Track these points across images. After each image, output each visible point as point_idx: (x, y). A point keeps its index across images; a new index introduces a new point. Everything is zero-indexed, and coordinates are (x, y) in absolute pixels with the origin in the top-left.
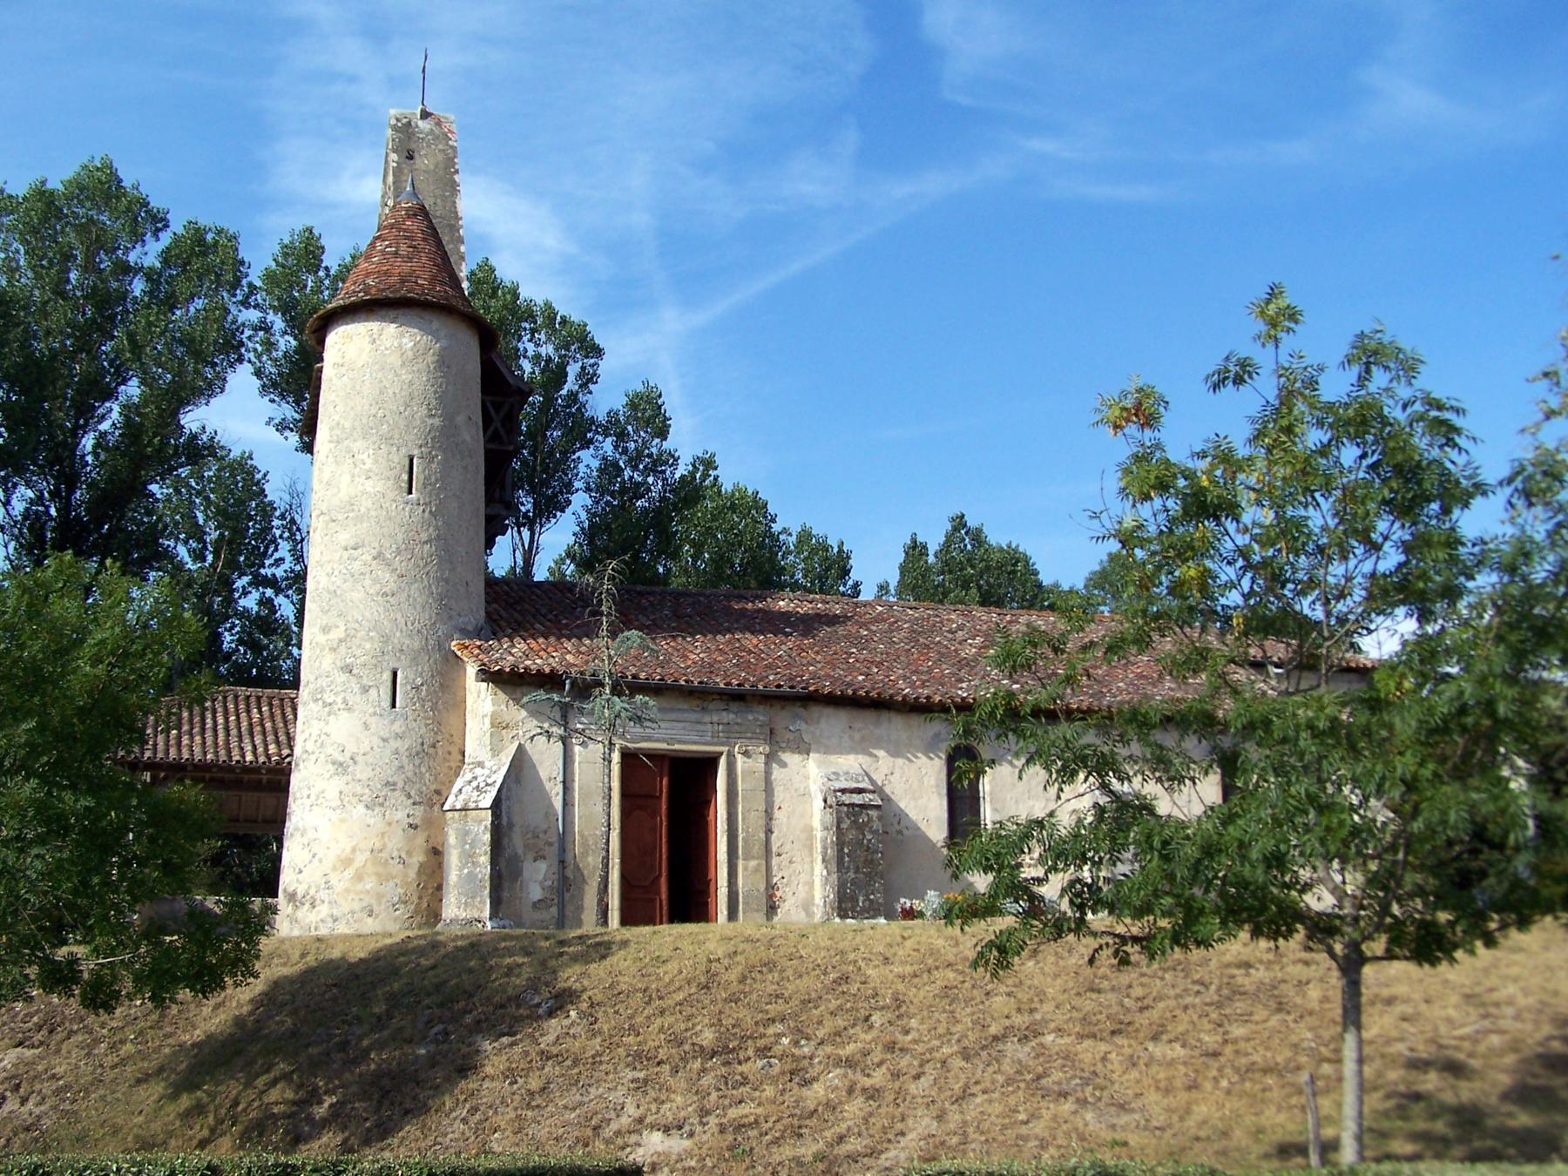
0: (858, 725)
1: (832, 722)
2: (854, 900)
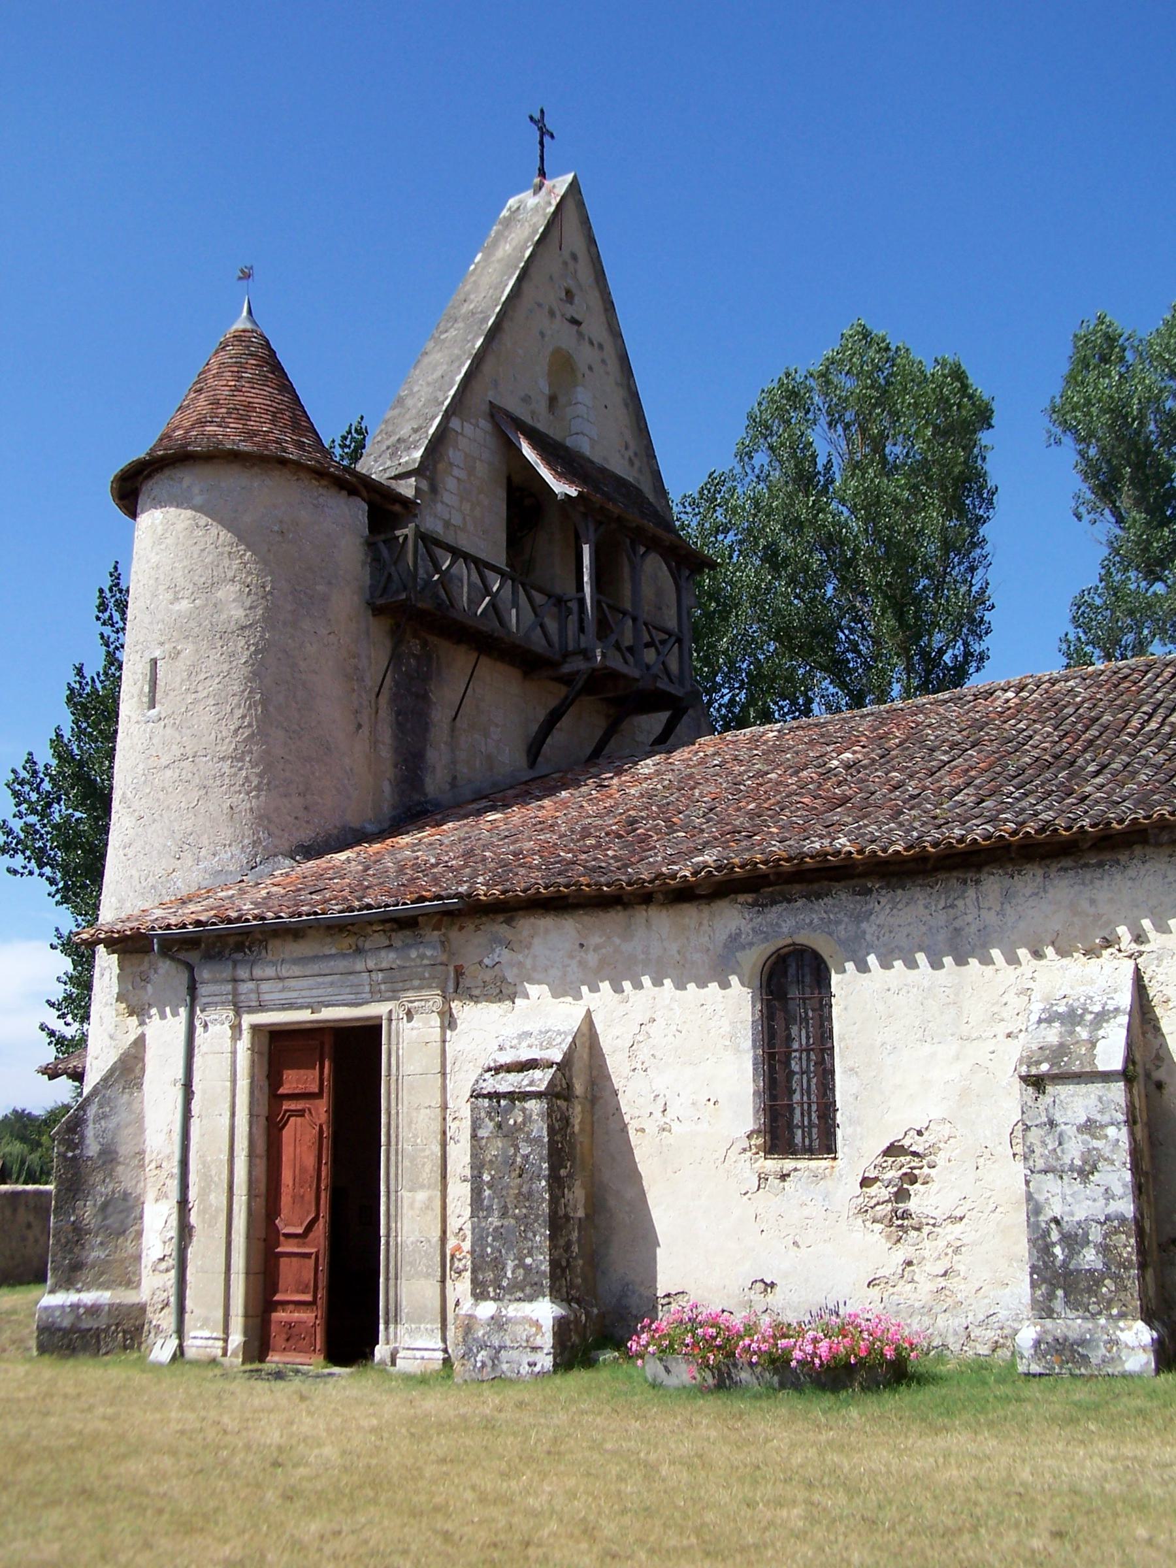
0: (596, 940)
1: (553, 936)
2: (498, 1264)
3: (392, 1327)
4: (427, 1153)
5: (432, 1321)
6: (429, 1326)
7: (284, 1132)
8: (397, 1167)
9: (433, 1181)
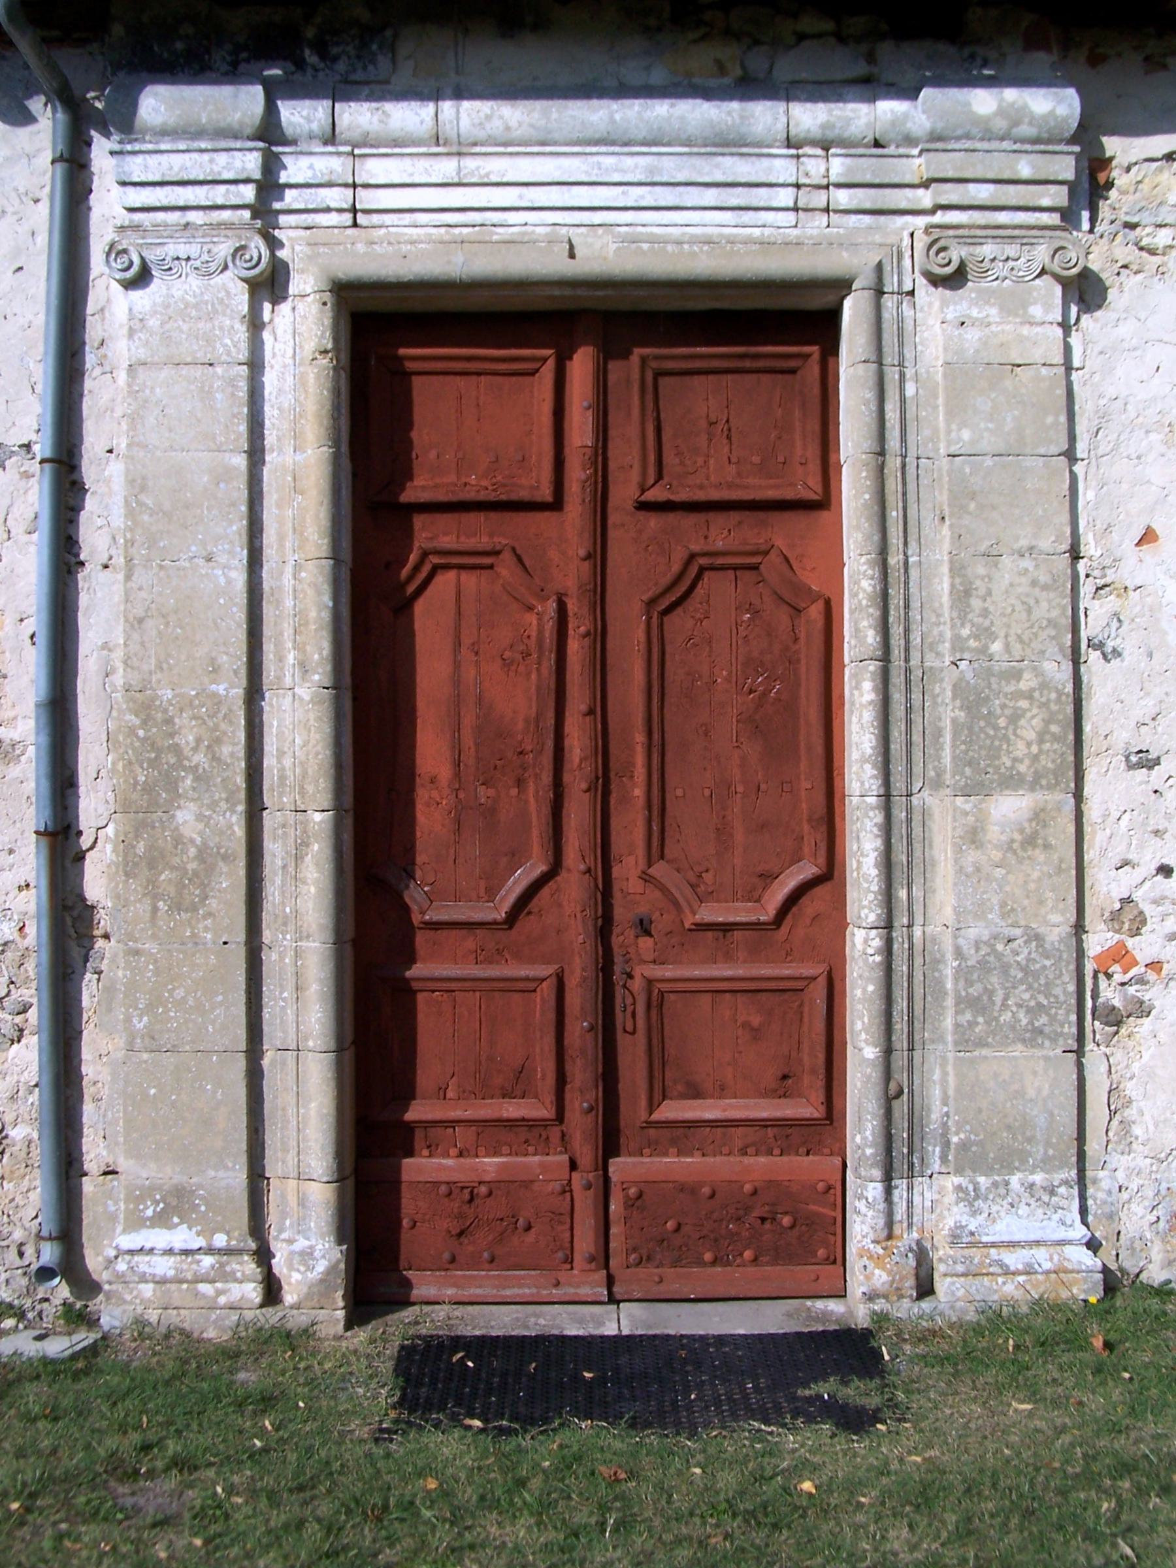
3: (901, 1185)
4: (1027, 682)
5: (1046, 1164)
6: (1038, 1178)
7: (419, 607)
8: (909, 722)
9: (1046, 762)
